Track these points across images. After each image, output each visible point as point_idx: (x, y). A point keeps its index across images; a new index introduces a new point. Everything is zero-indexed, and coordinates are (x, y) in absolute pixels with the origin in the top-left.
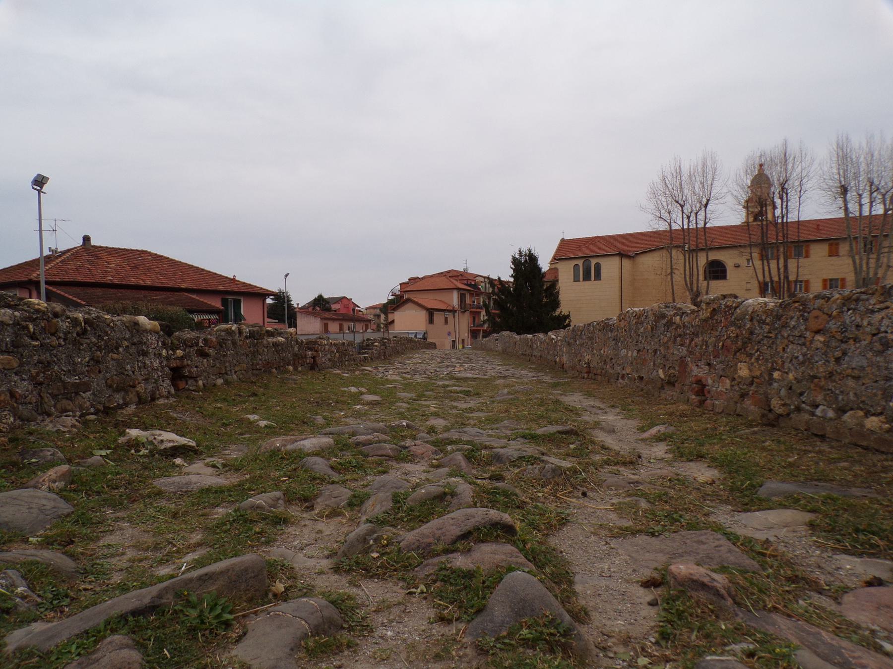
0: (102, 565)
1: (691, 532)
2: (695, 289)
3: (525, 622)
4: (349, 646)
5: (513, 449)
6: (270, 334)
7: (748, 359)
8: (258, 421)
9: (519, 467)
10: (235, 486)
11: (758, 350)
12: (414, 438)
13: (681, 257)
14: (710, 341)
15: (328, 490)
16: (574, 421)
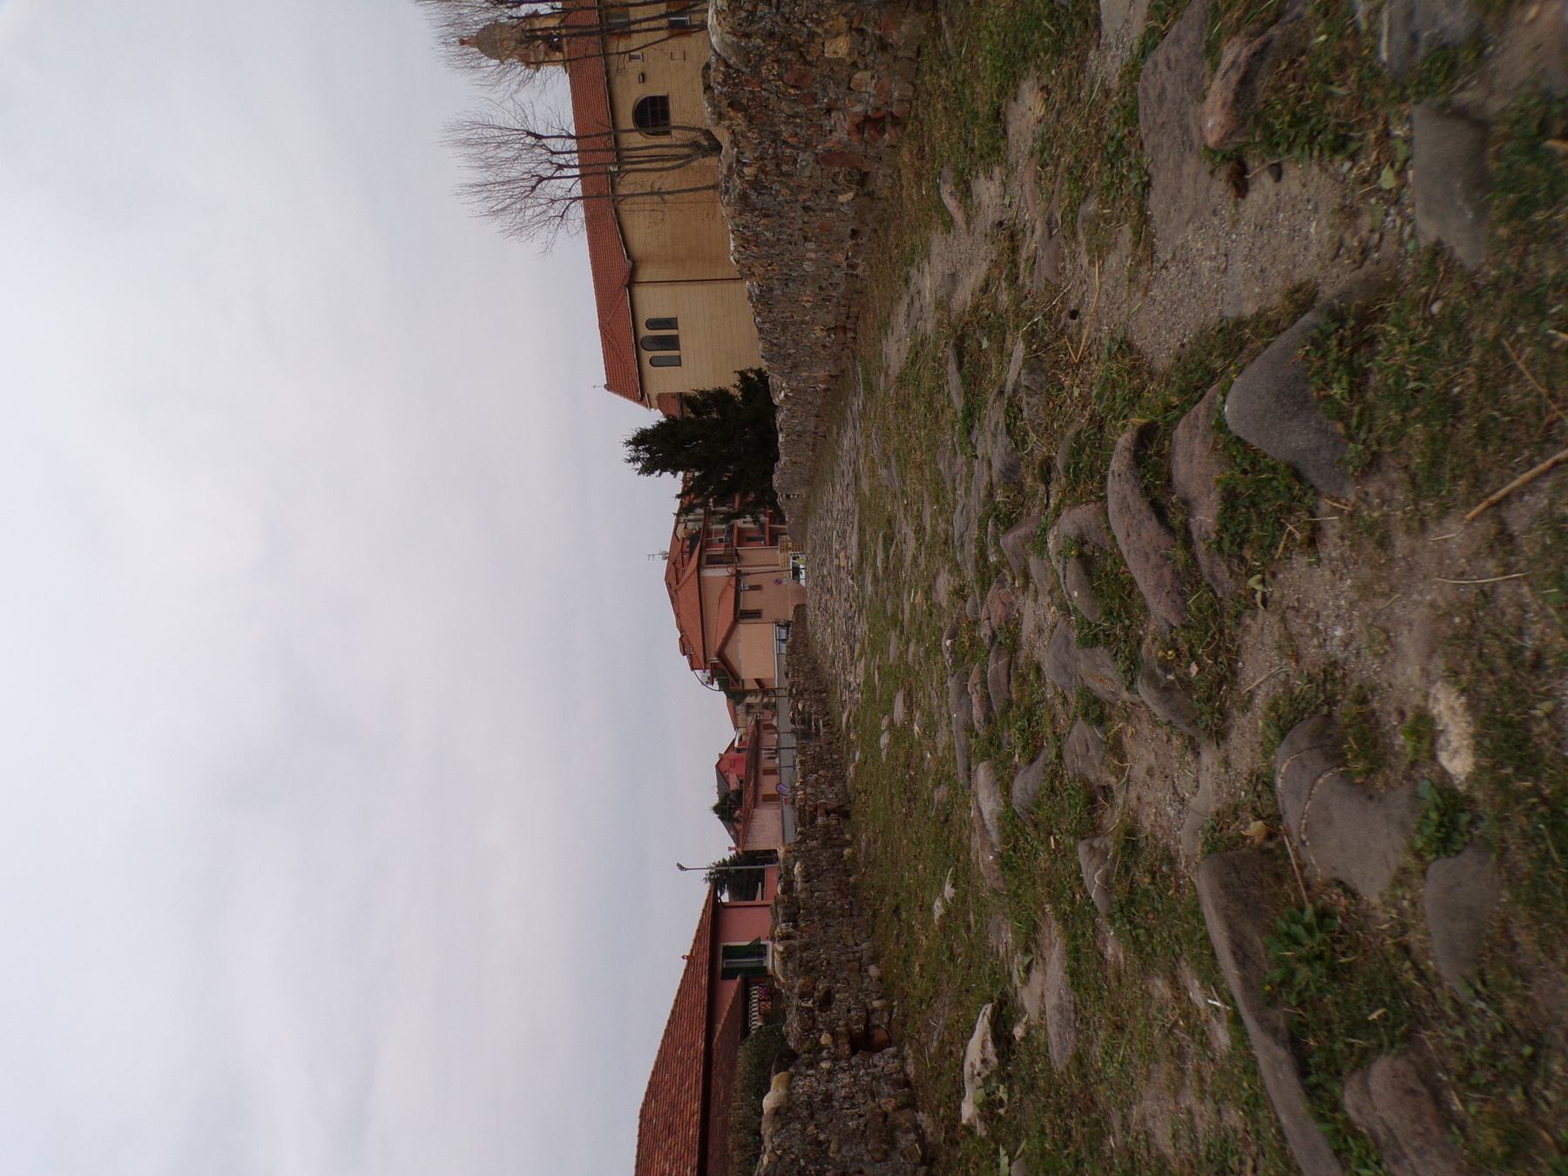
0: (1210, 1145)
1: (1141, 117)
2: (686, 151)
3: (1319, 390)
4: (1363, 701)
5: (993, 447)
6: (789, 887)
7: (818, 40)
8: (944, 900)
9: (1027, 434)
10: (1066, 927)
11: (801, 22)
12: (976, 623)
13: (631, 177)
14: (787, 110)
15: (1074, 763)
16: (937, 346)
